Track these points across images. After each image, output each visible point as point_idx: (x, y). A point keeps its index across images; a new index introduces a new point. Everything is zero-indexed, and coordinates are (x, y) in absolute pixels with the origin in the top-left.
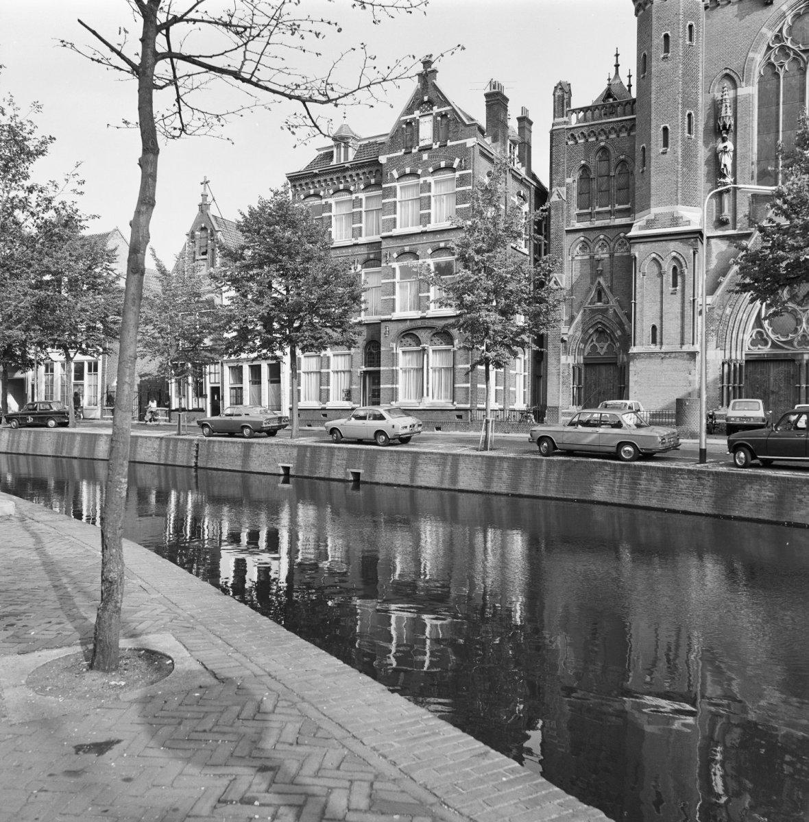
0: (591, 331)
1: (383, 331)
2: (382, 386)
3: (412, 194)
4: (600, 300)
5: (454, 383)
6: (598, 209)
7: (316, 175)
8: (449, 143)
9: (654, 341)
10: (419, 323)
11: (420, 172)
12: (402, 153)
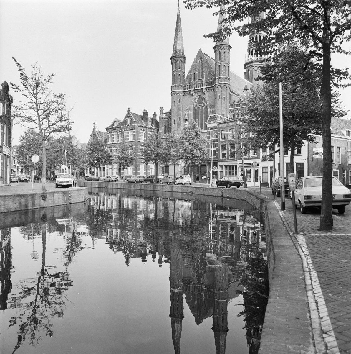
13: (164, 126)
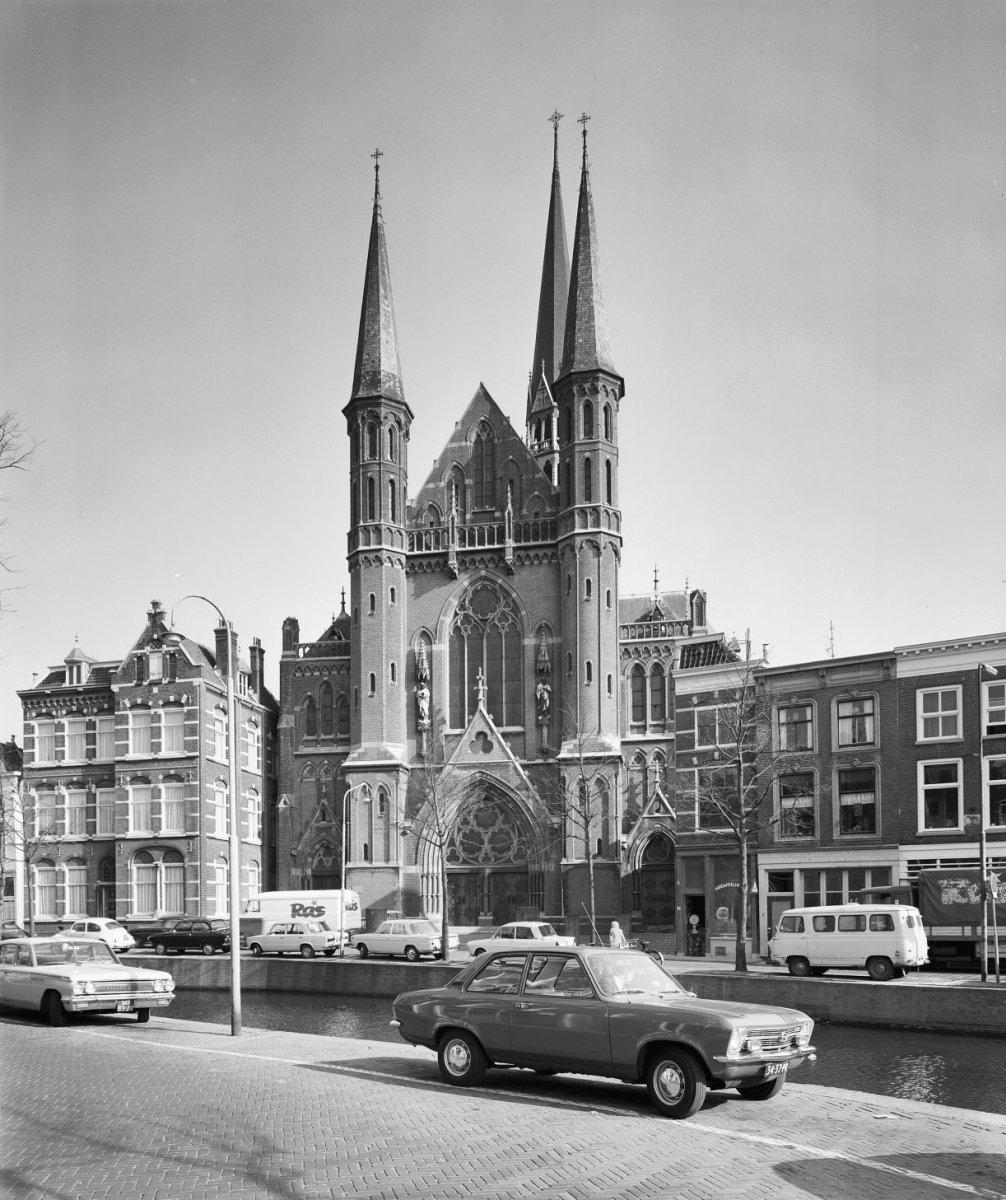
0: (317, 847)
1: (117, 848)
2: (117, 900)
3: (143, 723)
4: (324, 820)
5: (185, 896)
6: (323, 737)
7: (48, 695)
8: (177, 680)
9: (366, 858)
10: (152, 843)
11: (150, 703)
12: (132, 685)
13: (307, 703)
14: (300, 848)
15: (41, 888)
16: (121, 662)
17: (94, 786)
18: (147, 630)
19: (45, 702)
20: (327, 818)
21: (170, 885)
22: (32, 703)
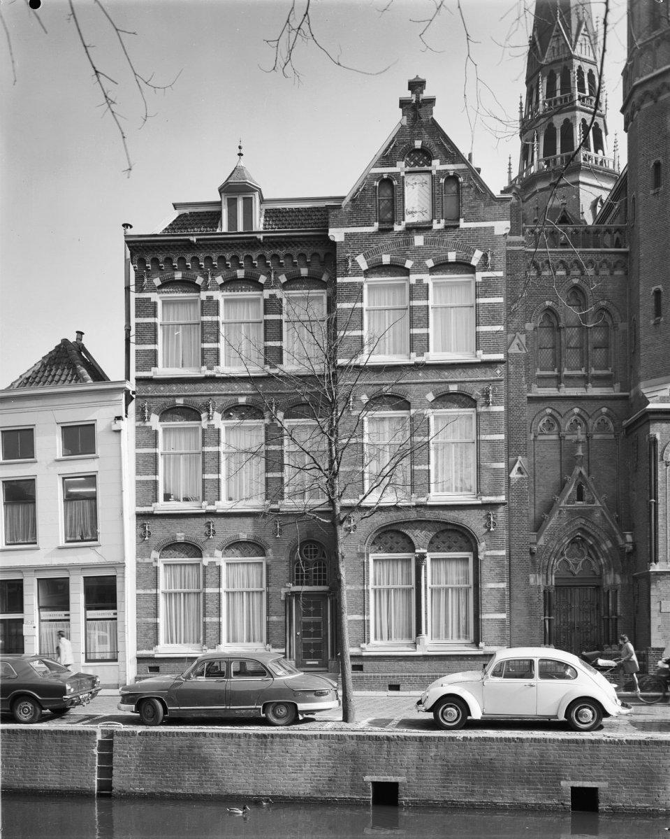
4: (580, 498)
8: (463, 224)
10: (413, 515)
11: (409, 264)
14: (541, 542)
15: (168, 595)
16: (343, 198)
17: (280, 415)
18: (401, 131)
19: (182, 260)
20: (586, 497)
21: (233, 593)
22: (155, 261)
